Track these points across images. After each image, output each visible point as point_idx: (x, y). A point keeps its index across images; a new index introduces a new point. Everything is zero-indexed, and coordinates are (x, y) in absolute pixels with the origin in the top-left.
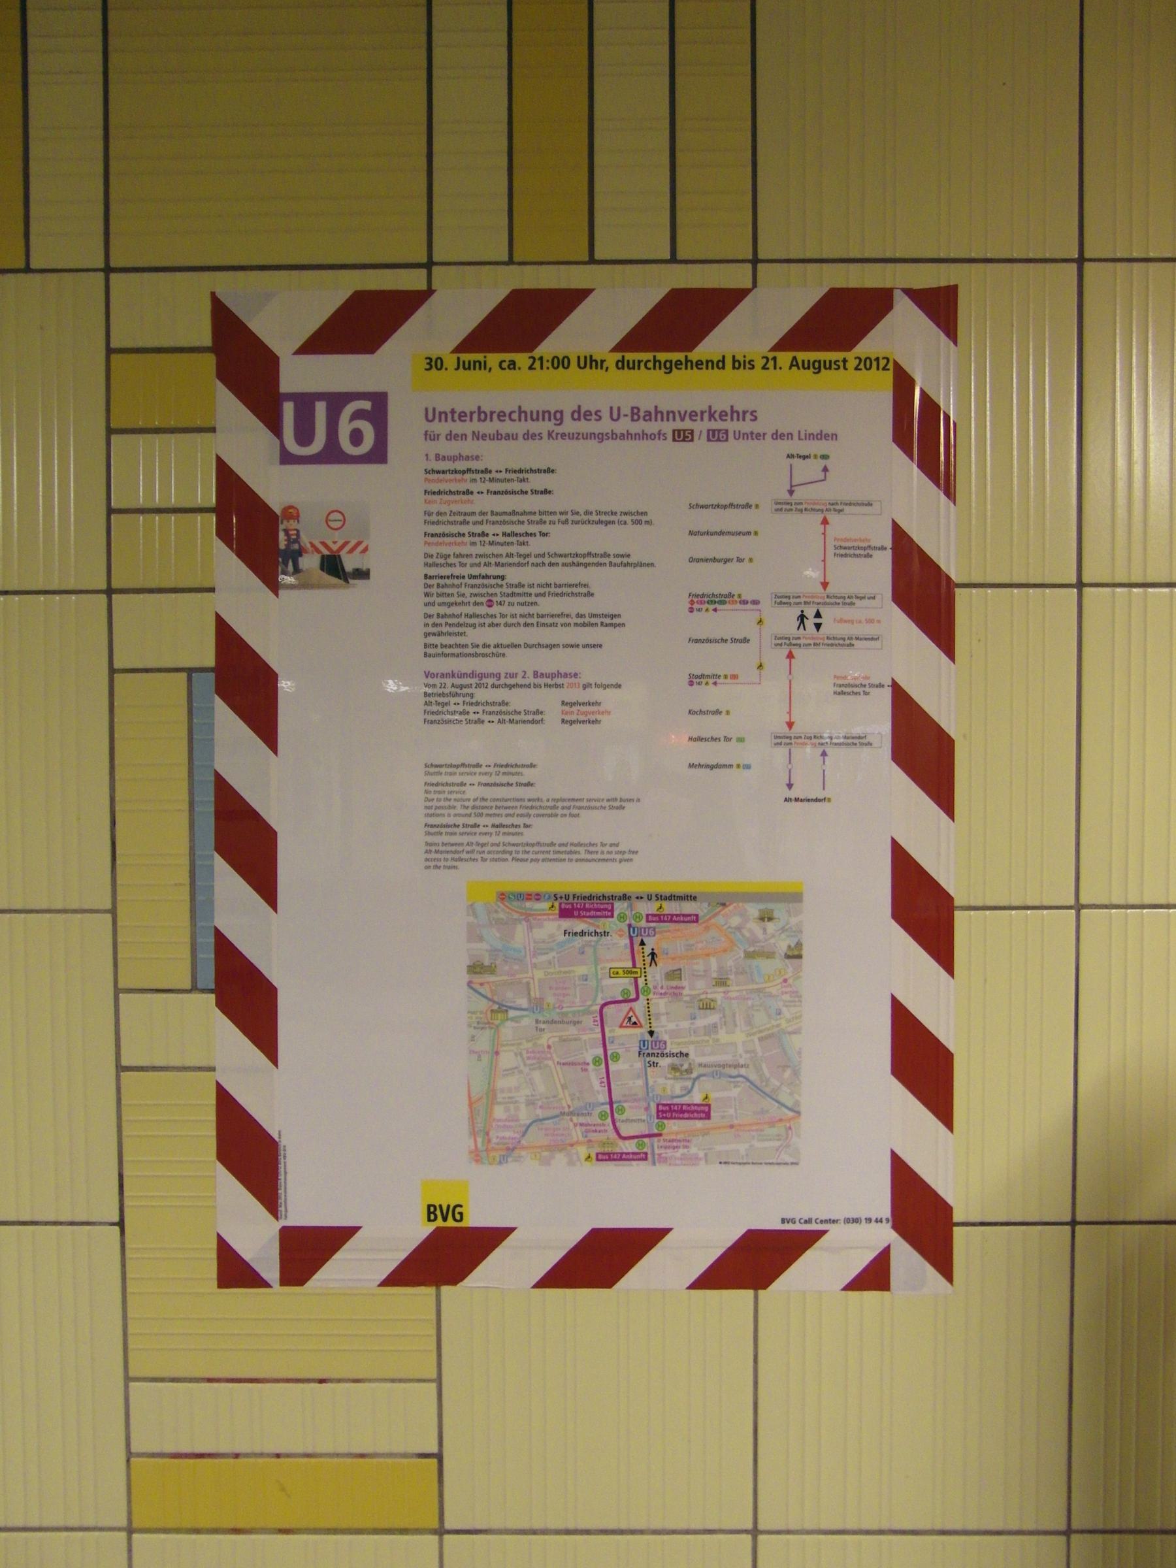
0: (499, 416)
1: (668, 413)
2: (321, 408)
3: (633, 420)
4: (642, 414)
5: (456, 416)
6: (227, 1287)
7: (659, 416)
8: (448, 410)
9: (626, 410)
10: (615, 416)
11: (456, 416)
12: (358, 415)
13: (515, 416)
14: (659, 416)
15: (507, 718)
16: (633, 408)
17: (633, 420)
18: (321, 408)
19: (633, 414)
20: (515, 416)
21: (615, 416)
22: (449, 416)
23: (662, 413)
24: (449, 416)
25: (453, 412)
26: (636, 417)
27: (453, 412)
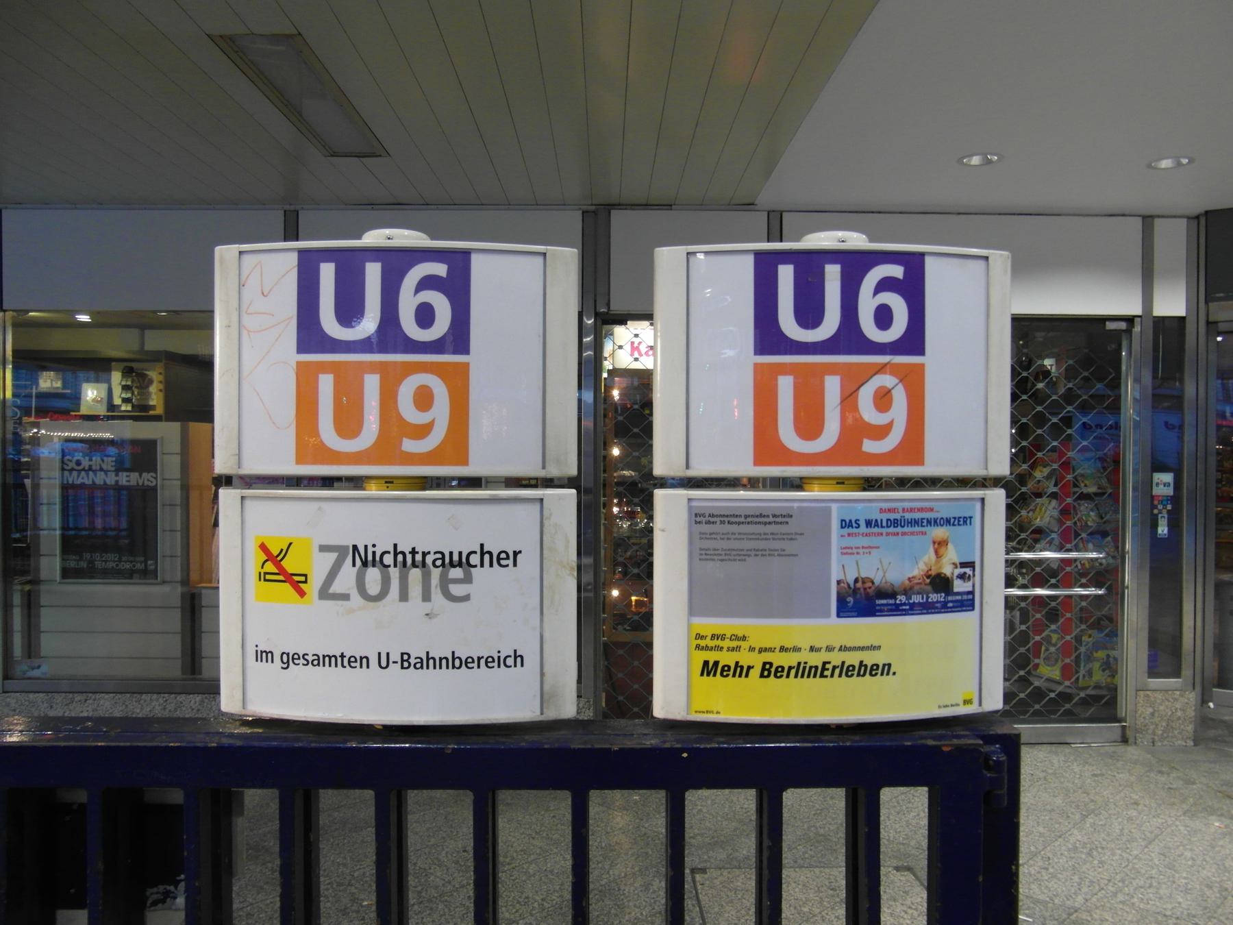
0: (487, 662)
1: (441, 659)
2: (833, 273)
3: (402, 667)
4: (412, 661)
5: (346, 660)
6: (923, 458)
7: (431, 662)
8: (338, 655)
9: (395, 656)
10: (384, 664)
11: (346, 660)
12: (885, 285)
13: (510, 661)
14: (431, 662)
15: (726, 519)
16: (402, 654)
17: (402, 667)
18: (833, 273)
19: (403, 661)
20: (510, 661)
21: (384, 664)
22: (339, 660)
23: (434, 659)
24: (339, 660)
25: (342, 656)
26: (766, 673)
27: (342, 656)
